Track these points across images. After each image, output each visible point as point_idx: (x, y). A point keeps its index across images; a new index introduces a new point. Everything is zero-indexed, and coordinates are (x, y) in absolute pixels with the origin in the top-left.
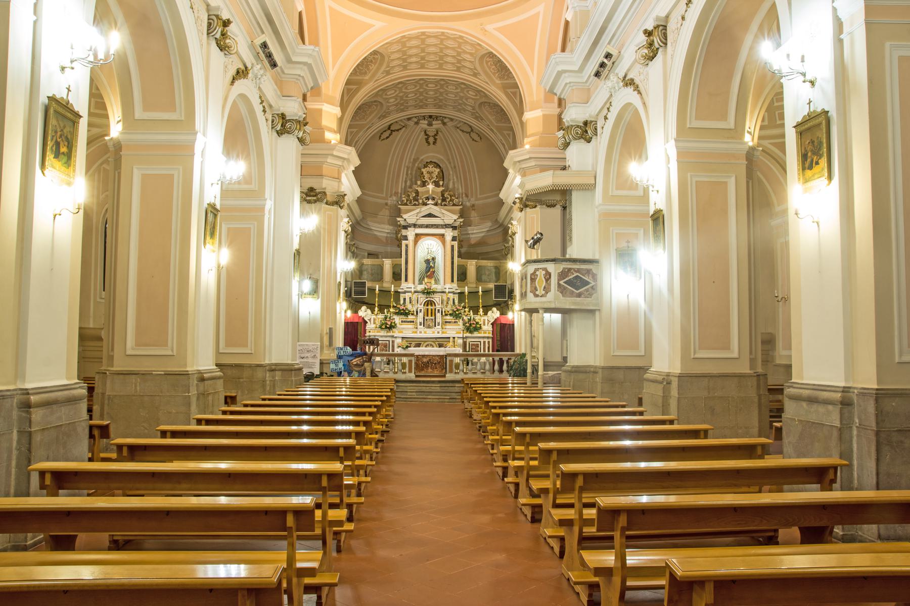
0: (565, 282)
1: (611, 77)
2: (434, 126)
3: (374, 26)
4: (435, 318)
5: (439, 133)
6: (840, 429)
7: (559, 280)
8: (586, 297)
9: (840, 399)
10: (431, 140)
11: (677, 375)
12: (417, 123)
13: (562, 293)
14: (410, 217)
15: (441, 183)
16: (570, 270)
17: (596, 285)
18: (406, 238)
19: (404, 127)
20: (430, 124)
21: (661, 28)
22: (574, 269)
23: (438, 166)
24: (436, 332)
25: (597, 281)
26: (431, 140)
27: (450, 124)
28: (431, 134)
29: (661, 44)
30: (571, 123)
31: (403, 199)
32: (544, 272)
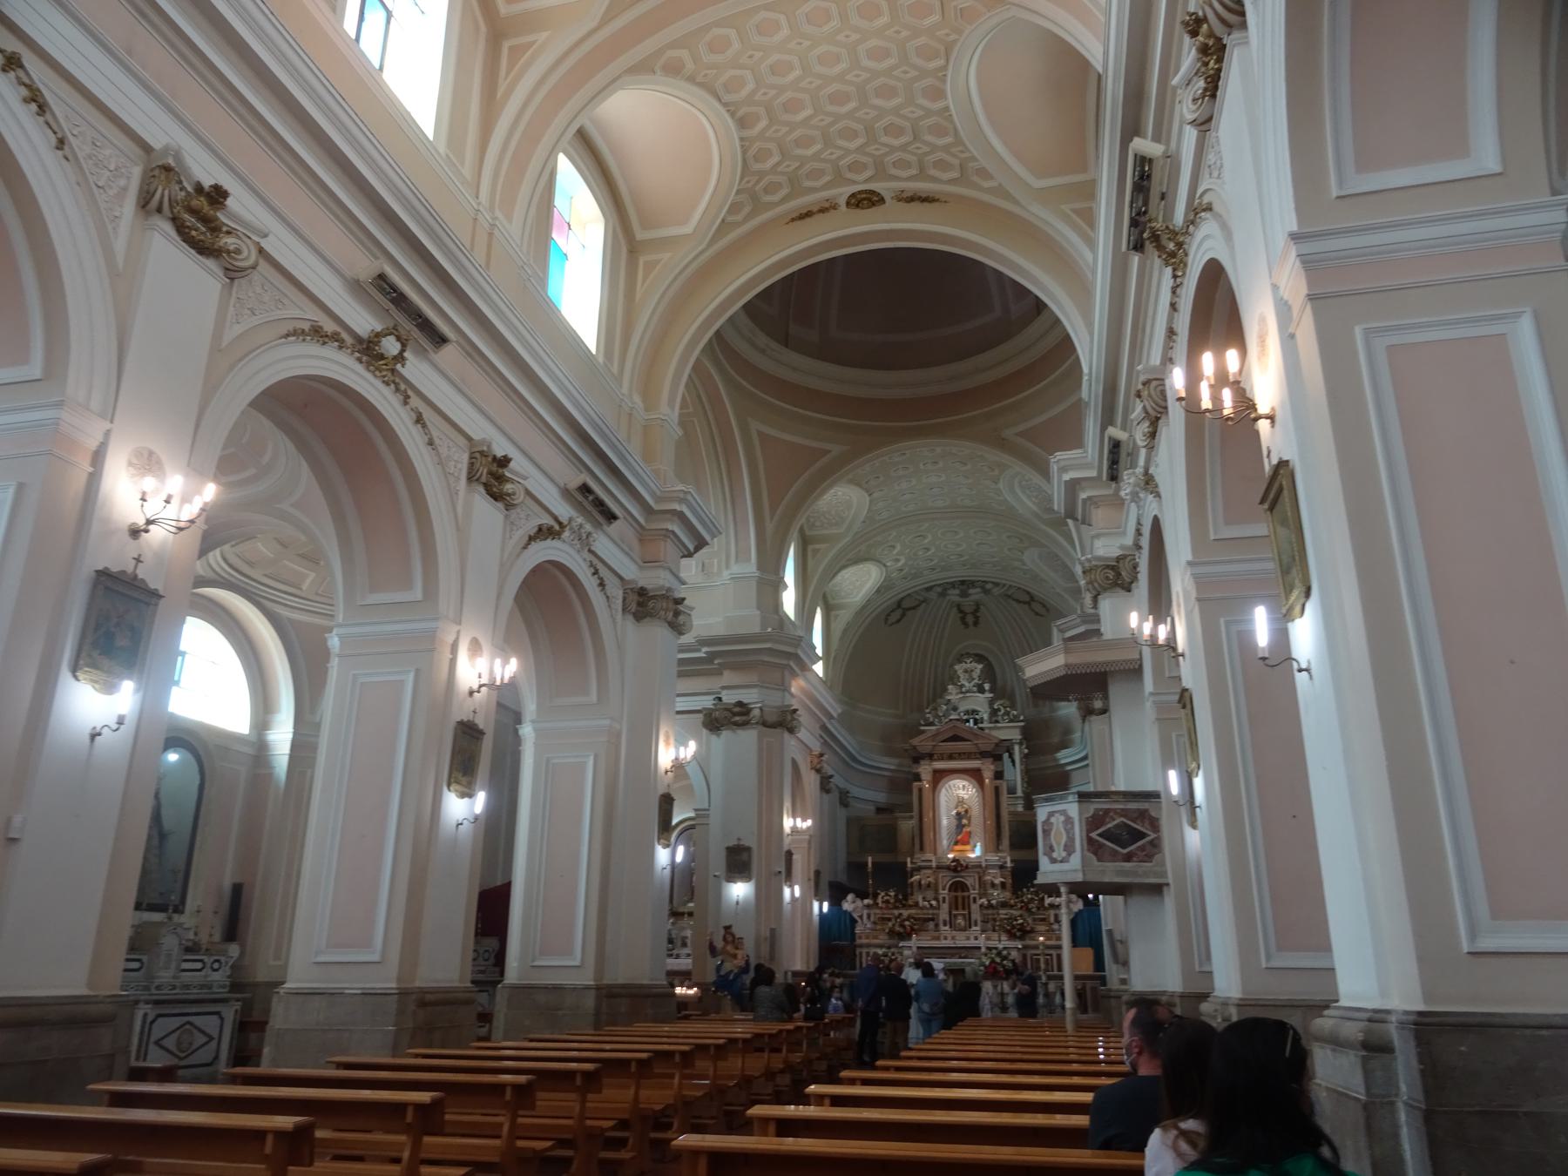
0: (1099, 835)
1: (1125, 478)
2: (973, 598)
3: (830, 451)
4: (970, 913)
5: (982, 607)
6: (1366, 1107)
7: (1089, 831)
8: (1140, 862)
9: (1360, 1036)
10: (970, 619)
11: (1236, 1002)
12: (943, 594)
13: (1095, 854)
14: (922, 743)
15: (987, 686)
16: (1107, 811)
17: (1158, 838)
18: (918, 778)
19: (923, 602)
20: (964, 594)
21: (1154, 383)
22: (1115, 810)
23: (980, 658)
24: (972, 937)
25: (1159, 831)
26: (970, 619)
27: (996, 591)
28: (968, 609)
29: (1160, 410)
30: (1094, 563)
31: (928, 715)
32: (1062, 818)
